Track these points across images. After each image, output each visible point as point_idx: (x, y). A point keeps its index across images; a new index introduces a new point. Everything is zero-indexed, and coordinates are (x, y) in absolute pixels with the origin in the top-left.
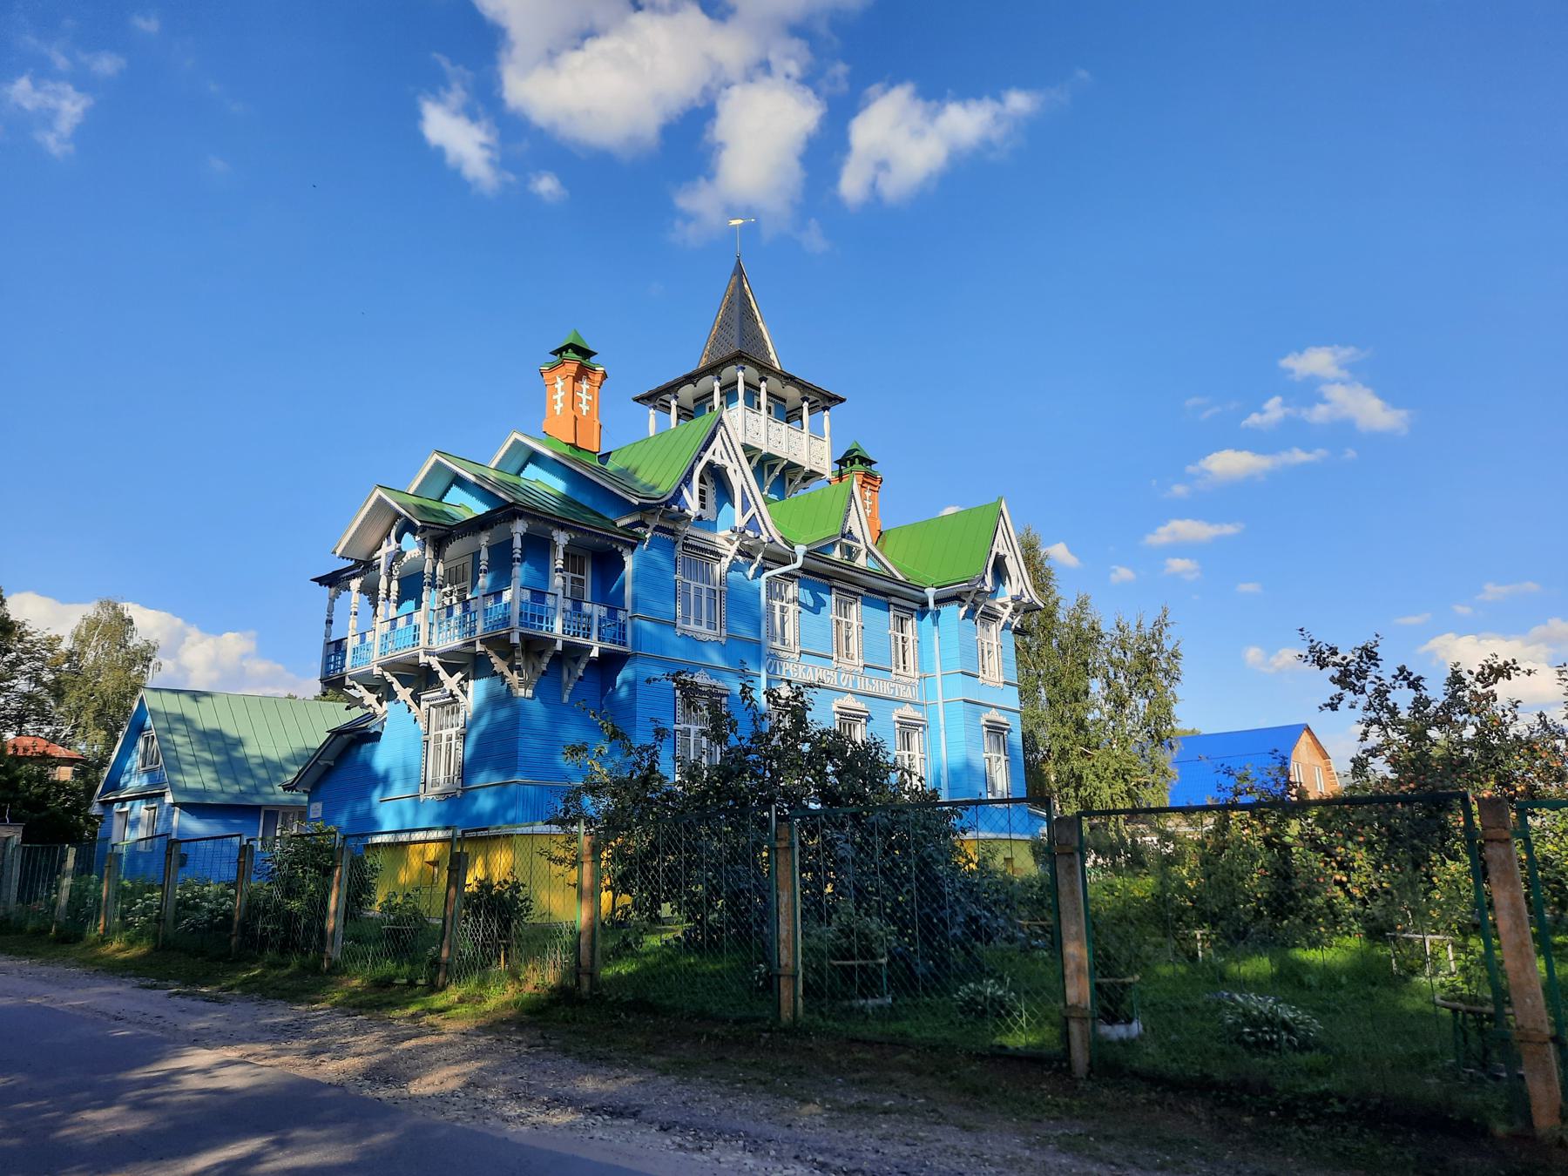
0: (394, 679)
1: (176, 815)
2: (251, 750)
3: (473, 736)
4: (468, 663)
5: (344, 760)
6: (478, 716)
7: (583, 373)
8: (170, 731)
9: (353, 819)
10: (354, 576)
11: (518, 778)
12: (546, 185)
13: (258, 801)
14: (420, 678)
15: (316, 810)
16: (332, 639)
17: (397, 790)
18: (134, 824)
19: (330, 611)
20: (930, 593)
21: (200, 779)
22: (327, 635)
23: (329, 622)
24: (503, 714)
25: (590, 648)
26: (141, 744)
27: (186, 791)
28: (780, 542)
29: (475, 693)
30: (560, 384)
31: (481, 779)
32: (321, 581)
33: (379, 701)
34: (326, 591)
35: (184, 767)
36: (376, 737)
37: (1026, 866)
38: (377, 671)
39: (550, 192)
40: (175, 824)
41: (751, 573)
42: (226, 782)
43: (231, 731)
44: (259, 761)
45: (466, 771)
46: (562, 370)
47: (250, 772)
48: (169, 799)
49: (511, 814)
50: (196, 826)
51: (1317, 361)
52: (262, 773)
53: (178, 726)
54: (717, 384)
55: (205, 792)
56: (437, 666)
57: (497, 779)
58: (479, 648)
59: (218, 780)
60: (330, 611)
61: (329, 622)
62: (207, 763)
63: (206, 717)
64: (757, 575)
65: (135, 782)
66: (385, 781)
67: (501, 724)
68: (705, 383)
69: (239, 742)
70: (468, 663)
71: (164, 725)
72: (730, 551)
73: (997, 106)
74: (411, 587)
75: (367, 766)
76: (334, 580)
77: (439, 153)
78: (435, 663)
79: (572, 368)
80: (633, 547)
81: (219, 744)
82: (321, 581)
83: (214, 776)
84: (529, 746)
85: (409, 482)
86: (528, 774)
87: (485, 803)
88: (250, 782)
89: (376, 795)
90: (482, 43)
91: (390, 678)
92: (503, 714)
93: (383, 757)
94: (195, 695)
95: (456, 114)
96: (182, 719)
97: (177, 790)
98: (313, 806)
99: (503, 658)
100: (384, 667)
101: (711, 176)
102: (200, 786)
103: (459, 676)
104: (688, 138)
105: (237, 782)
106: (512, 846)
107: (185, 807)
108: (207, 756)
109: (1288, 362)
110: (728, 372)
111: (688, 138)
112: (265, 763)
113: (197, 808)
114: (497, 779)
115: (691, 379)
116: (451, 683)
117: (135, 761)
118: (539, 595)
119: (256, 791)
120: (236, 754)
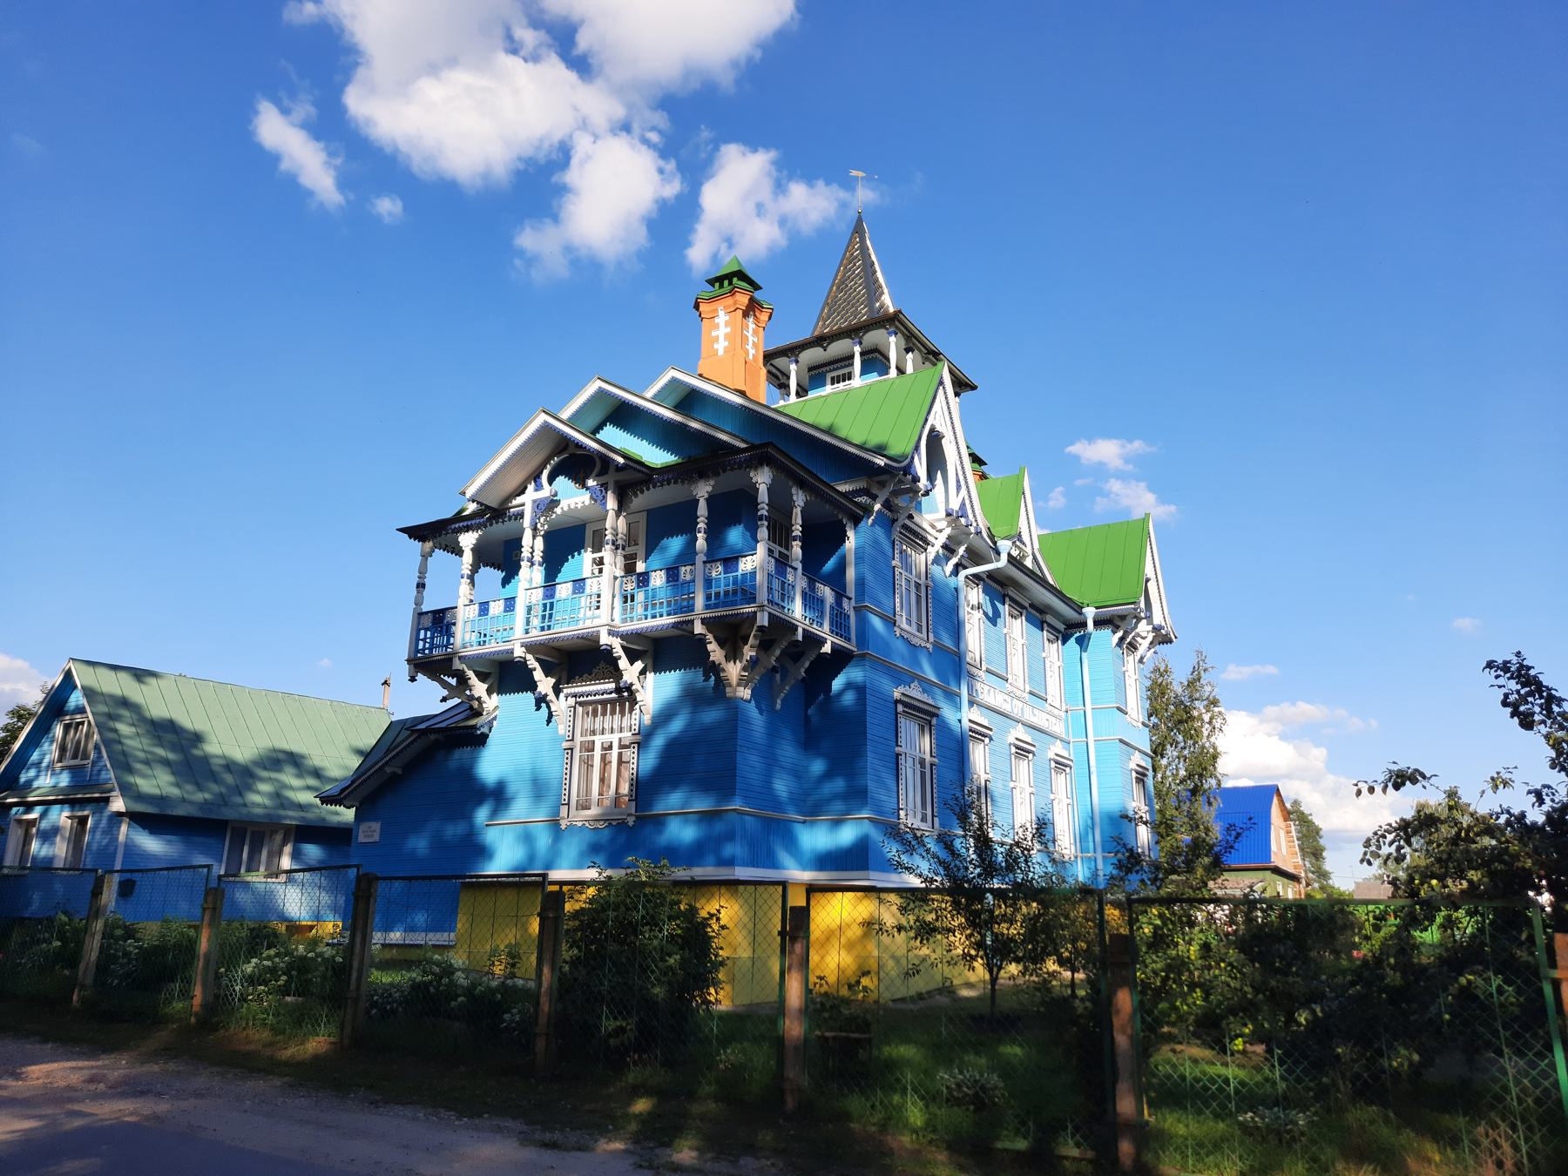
0: (537, 665)
1: (124, 828)
2: (212, 748)
3: (659, 741)
4: (657, 651)
5: (425, 769)
6: (663, 717)
7: (753, 307)
8: (111, 717)
9: (439, 844)
10: (467, 529)
11: (737, 804)
12: (387, 207)
13: (228, 814)
14: (577, 660)
15: (371, 832)
16: (427, 607)
17: (520, 808)
18: (48, 836)
19: (422, 572)
20: (1090, 613)
21: (158, 783)
22: (418, 603)
23: (421, 586)
24: (712, 715)
25: (822, 642)
26: (58, 730)
27: (140, 797)
28: (985, 534)
29: (656, 690)
30: (722, 318)
31: (672, 801)
32: (417, 533)
33: (489, 692)
34: (416, 546)
35: (138, 766)
36: (482, 740)
37: (504, 858)
38: (519, 652)
39: (390, 214)
40: (122, 838)
41: (949, 567)
42: (189, 787)
43: (187, 722)
44: (222, 762)
45: (645, 789)
46: (729, 301)
47: (213, 776)
48: (118, 805)
49: (729, 850)
50: (151, 844)
51: (1106, 451)
52: (229, 778)
53: (125, 713)
54: (857, 349)
55: (161, 800)
56: (618, 651)
57: (702, 804)
58: (699, 629)
59: (177, 785)
60: (422, 572)
61: (421, 586)
62: (166, 763)
63: (157, 702)
64: (955, 572)
65: (46, 781)
66: (498, 796)
67: (708, 729)
68: (837, 348)
69: (197, 738)
70: (657, 651)
71: (103, 709)
72: (938, 541)
73: (842, 194)
74: (565, 542)
75: (467, 775)
76: (435, 533)
77: (274, 158)
78: (617, 645)
79: (743, 299)
80: (856, 521)
81: (170, 737)
82: (417, 533)
83: (171, 778)
84: (750, 764)
85: (646, 388)
86: (747, 799)
87: (683, 833)
88: (215, 788)
89: (482, 814)
90: (321, 65)
91: (532, 662)
92: (712, 715)
93: (491, 765)
94: (140, 675)
95: (294, 125)
96: (124, 702)
97: (127, 790)
98: (363, 827)
99: (721, 644)
100: (530, 648)
101: (555, 219)
102: (156, 791)
103: (639, 665)
104: (540, 182)
105: (201, 788)
106: (735, 894)
107: (139, 819)
108: (160, 752)
109: (1077, 448)
110: (873, 337)
111: (540, 182)
112: (230, 766)
113: (154, 819)
114: (702, 804)
115: (820, 341)
116: (630, 671)
117: (49, 751)
118: (782, 563)
119: (223, 800)
120: (196, 752)
